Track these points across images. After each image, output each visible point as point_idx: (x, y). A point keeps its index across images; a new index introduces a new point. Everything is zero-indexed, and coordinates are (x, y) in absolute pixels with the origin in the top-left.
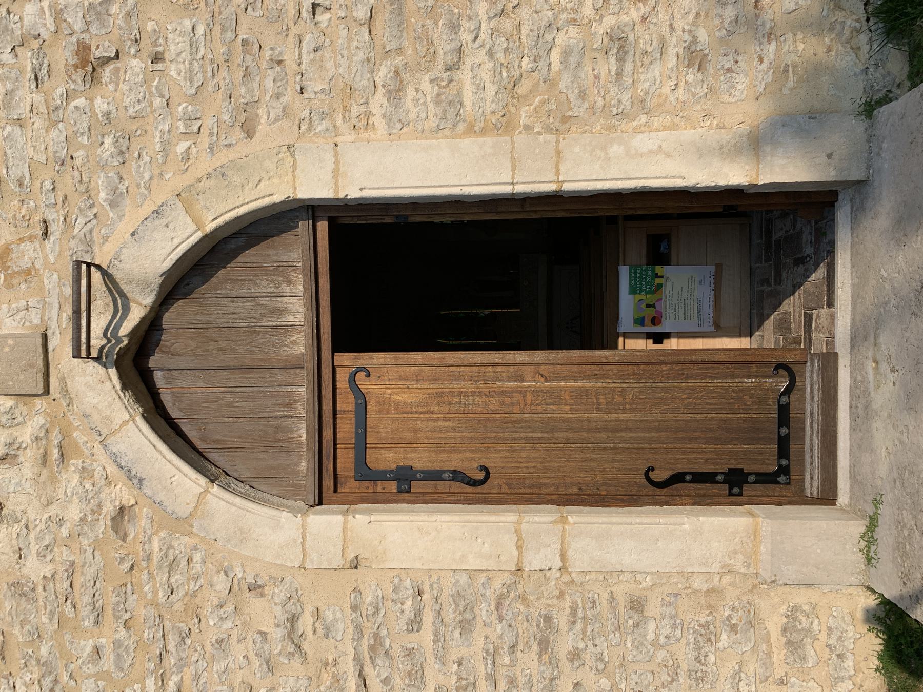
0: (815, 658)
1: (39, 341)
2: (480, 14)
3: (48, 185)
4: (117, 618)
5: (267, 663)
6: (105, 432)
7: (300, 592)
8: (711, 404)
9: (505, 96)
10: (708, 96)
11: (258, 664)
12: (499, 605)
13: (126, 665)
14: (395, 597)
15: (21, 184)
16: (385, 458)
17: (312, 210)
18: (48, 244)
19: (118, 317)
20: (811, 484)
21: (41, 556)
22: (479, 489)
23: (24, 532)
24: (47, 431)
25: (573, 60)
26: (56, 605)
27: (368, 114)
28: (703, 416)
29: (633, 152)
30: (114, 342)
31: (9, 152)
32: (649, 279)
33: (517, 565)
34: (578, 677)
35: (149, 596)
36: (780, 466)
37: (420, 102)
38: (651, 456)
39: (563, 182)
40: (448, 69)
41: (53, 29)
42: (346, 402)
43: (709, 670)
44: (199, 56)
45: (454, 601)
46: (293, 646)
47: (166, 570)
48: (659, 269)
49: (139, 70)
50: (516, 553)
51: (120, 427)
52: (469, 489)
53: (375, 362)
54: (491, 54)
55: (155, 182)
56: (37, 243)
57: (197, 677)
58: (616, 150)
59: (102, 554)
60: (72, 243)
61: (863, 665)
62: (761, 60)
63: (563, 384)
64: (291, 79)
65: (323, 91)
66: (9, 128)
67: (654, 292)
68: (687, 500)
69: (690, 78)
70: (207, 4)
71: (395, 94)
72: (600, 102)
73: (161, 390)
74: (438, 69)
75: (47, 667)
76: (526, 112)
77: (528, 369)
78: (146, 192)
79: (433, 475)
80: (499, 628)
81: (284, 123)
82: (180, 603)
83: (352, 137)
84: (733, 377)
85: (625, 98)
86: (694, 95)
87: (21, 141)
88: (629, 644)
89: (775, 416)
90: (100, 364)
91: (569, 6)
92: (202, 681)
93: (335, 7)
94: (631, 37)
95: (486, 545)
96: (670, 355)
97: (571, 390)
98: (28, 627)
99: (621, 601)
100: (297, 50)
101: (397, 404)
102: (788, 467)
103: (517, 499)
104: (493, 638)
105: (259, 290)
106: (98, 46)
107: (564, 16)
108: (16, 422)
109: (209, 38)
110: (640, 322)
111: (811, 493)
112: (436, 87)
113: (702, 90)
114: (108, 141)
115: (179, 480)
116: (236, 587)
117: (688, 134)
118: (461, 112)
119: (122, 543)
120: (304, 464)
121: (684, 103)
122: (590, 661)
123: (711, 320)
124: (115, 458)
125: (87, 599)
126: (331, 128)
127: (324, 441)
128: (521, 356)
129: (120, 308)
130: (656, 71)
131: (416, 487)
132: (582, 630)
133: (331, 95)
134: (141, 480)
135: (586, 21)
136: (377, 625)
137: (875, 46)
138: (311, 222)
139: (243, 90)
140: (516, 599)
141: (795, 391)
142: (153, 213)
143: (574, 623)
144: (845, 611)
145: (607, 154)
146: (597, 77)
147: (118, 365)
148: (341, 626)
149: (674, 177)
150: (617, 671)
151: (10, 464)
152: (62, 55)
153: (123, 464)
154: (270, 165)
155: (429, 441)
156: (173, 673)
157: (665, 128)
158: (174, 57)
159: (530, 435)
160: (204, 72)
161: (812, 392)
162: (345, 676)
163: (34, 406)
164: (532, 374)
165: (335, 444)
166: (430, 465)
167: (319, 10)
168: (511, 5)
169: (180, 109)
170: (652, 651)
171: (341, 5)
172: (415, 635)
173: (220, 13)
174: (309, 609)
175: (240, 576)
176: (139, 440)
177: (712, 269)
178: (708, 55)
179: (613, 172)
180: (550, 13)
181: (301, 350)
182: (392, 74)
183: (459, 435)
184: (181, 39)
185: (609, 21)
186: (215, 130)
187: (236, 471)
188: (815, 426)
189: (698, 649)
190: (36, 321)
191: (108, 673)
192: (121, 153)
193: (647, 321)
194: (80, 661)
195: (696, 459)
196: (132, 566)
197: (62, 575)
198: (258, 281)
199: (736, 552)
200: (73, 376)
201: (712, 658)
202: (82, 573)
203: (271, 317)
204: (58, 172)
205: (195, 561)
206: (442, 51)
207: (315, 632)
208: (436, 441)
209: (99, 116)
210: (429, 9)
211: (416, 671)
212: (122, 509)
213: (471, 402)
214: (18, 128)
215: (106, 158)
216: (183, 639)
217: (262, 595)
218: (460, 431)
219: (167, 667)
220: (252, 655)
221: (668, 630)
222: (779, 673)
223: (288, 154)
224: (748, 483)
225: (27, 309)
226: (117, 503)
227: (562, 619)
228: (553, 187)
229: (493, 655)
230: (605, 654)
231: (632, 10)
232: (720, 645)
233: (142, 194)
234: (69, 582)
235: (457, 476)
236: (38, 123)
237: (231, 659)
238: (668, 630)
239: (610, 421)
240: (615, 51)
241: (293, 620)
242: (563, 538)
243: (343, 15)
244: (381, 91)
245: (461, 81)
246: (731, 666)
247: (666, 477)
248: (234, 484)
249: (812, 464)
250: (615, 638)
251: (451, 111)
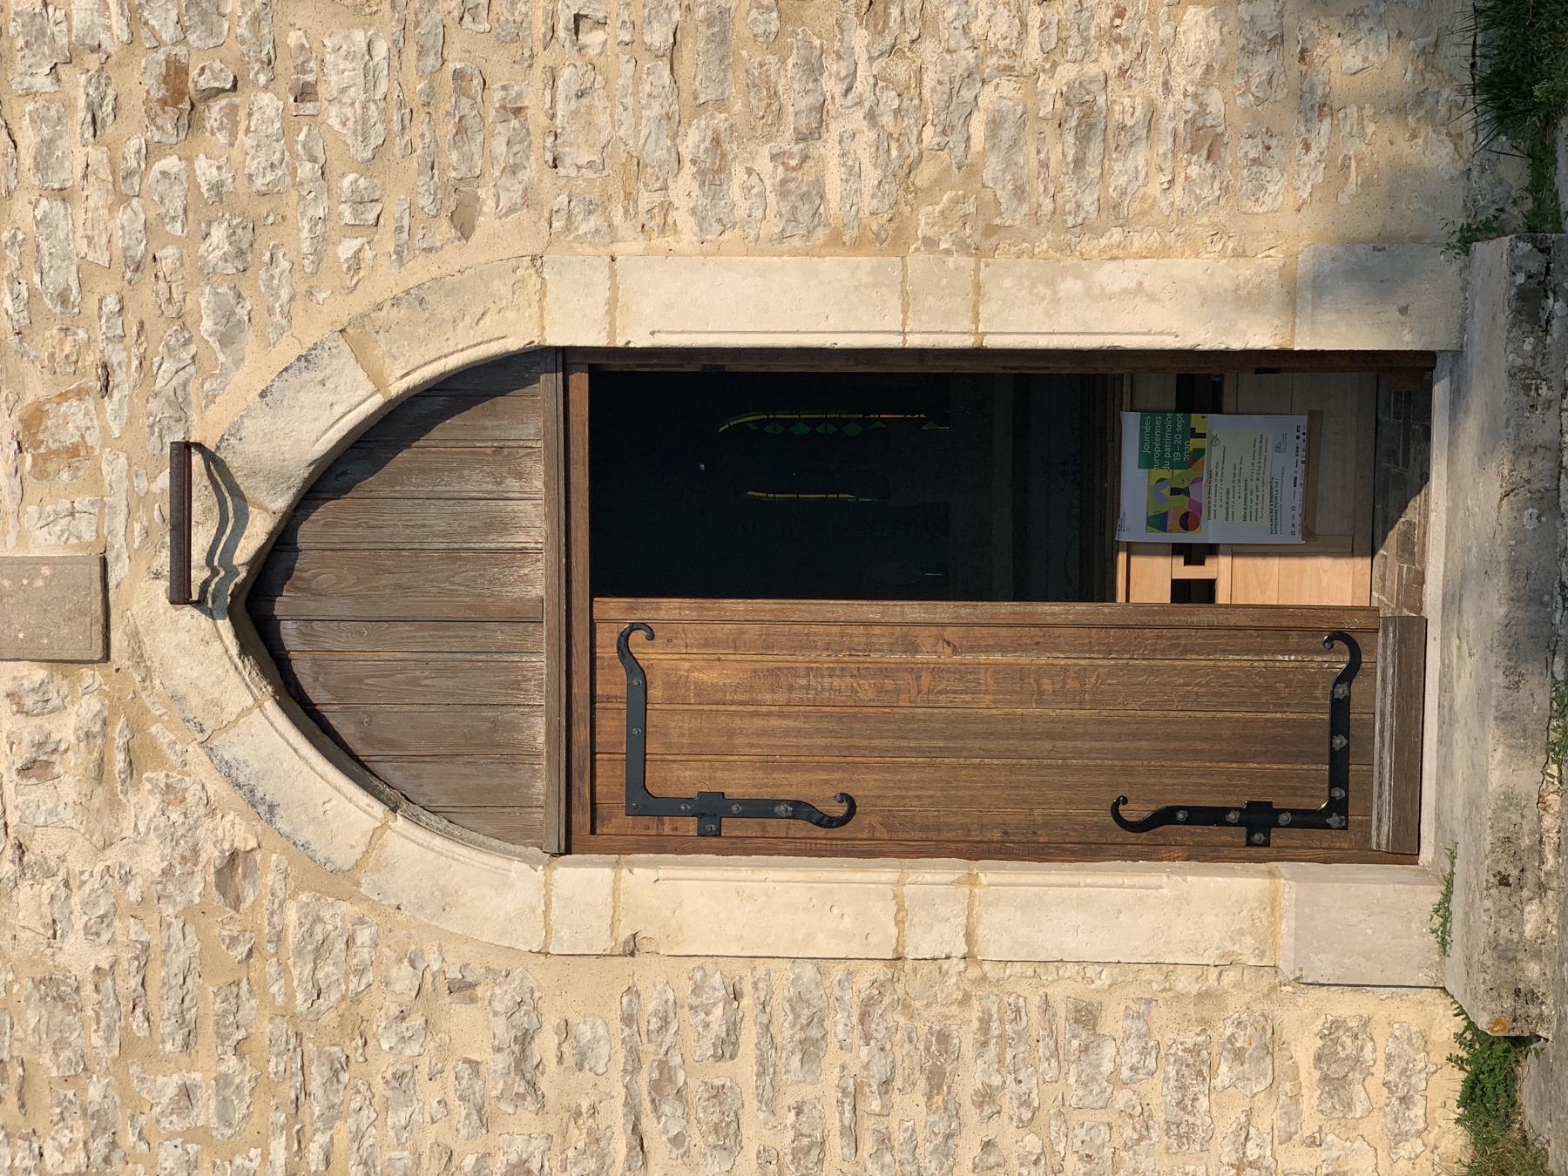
0: (1367, 1104)
1: (97, 570)
2: (857, 50)
3: (111, 304)
4: (223, 1038)
5: (479, 1111)
6: (209, 725)
7: (537, 995)
8: (1223, 695)
9: (894, 188)
10: (1222, 202)
11: (464, 1113)
12: (864, 1016)
13: (238, 1116)
14: (695, 1001)
15: (63, 298)
16: (678, 777)
17: (564, 358)
18: (109, 405)
19: (228, 531)
20: (1379, 828)
21: (91, 933)
22: (837, 832)
23: (63, 892)
24: (104, 723)
25: (1006, 135)
26: (116, 1016)
27: (667, 207)
28: (1210, 714)
29: (1097, 290)
30: (222, 573)
31: (44, 245)
32: (1178, 440)
33: (896, 950)
34: (990, 1131)
35: (280, 1000)
36: (1332, 800)
37: (754, 191)
38: (1123, 779)
39: (986, 333)
40: (801, 138)
41: (125, 37)
42: (612, 682)
43: (1199, 1122)
44: (379, 95)
45: (793, 1009)
46: (523, 1083)
47: (310, 957)
48: (1197, 420)
49: (273, 113)
50: (895, 931)
51: (238, 718)
52: (821, 832)
53: (663, 615)
54: (872, 117)
55: (298, 305)
56: (90, 403)
57: (358, 1136)
58: (1070, 286)
59: (197, 932)
60: (154, 405)
63: (983, 658)
64: (537, 142)
65: (591, 164)
66: (44, 203)
68: (1179, 851)
69: (1194, 171)
70: (393, 7)
71: (713, 175)
72: (1048, 205)
73: (292, 655)
74: (785, 140)
75: (99, 1121)
76: (928, 215)
77: (926, 632)
78: (284, 322)
79: (760, 809)
81: (523, 215)
82: (332, 1014)
83: (637, 246)
84: (1259, 652)
85: (1089, 200)
86: (1198, 199)
87: (64, 227)
88: (1072, 1080)
89: (1327, 717)
90: (202, 611)
91: (1002, 45)
92: (367, 1142)
93: (614, 23)
94: (1101, 100)
95: (846, 918)
96: (1156, 613)
97: (996, 669)
98: (66, 1054)
99: (1062, 1010)
100: (548, 92)
101: (700, 689)
103: (902, 848)
104: (854, 1068)
106: (203, 69)
107: (993, 61)
108: (50, 706)
109: (395, 63)
111: (1378, 845)
112: (781, 169)
114: (218, 233)
115: (337, 808)
116: (428, 987)
117: (1187, 267)
118: (822, 210)
119: (232, 913)
121: (1182, 211)
123: (1298, 521)
124: (227, 770)
125: (170, 1006)
126: (604, 228)
127: (575, 748)
129: (231, 515)
130: (1139, 157)
131: (731, 827)
132: (998, 1056)
133: (605, 173)
134: (272, 808)
135: (1028, 70)
136: (664, 1048)
137: (1481, 138)
138: (560, 375)
140: (892, 1006)
141: (1359, 676)
142: (299, 359)
143: (985, 1044)
144: (1414, 1029)
145: (1056, 293)
146: (1044, 165)
149: (1161, 333)
150: (1053, 1122)
151: (38, 777)
152: (140, 82)
153: (242, 779)
154: (501, 288)
155: (754, 751)
156: (317, 1130)
158: (335, 94)
159: (925, 744)
160: (388, 122)
161: (1384, 680)
162: (608, 1134)
163: (80, 680)
164: (932, 640)
165: (593, 754)
166: (755, 790)
167: (584, 25)
168: (908, 38)
170: (1109, 1090)
171: (624, 22)
172: (726, 1065)
173: (417, 24)
174: (551, 1021)
175: (435, 968)
176: (269, 739)
177: (1303, 420)
178: (1222, 134)
179: (1065, 322)
180: (970, 55)
181: (538, 590)
182: (707, 144)
183: (805, 742)
184: (349, 66)
185: (1067, 72)
186: (406, 222)
187: (424, 794)
188: (1387, 735)
189: (1182, 1088)
190: (88, 536)
191: (205, 1128)
192: (241, 253)
193: (1173, 521)
194: (158, 1109)
195: (1195, 784)
196: (251, 951)
197: (127, 964)
198: (466, 472)
199: (1241, 933)
200: (155, 631)
201: (1203, 1103)
202: (164, 963)
203: (488, 534)
204: (130, 282)
205: (359, 942)
206: (791, 109)
207: (560, 1060)
208: (766, 751)
209: (204, 189)
210: (772, 37)
211: (728, 1124)
212: (234, 855)
213: (827, 685)
214: (60, 204)
215: (214, 261)
216: (336, 1073)
217: (473, 1000)
218: (808, 735)
219: (308, 1120)
220: (452, 1099)
221: (1135, 1058)
222: (1309, 1127)
223: (532, 271)
224: (1279, 826)
225: (72, 514)
226: (227, 846)
227: (965, 1039)
228: (967, 342)
229: (854, 1095)
230: (1034, 1095)
231: (1104, 55)
232: (1217, 1082)
233: (277, 326)
234: (139, 978)
235: (800, 809)
236: (96, 196)
237: (416, 1106)
238: (1135, 1058)
240: (1074, 123)
241: (525, 1039)
242: (970, 906)
243: (627, 39)
244: (689, 169)
246: (1236, 1115)
247: (1147, 814)
248: (425, 817)
249: (1380, 796)
250: (1049, 1069)
251: (805, 210)
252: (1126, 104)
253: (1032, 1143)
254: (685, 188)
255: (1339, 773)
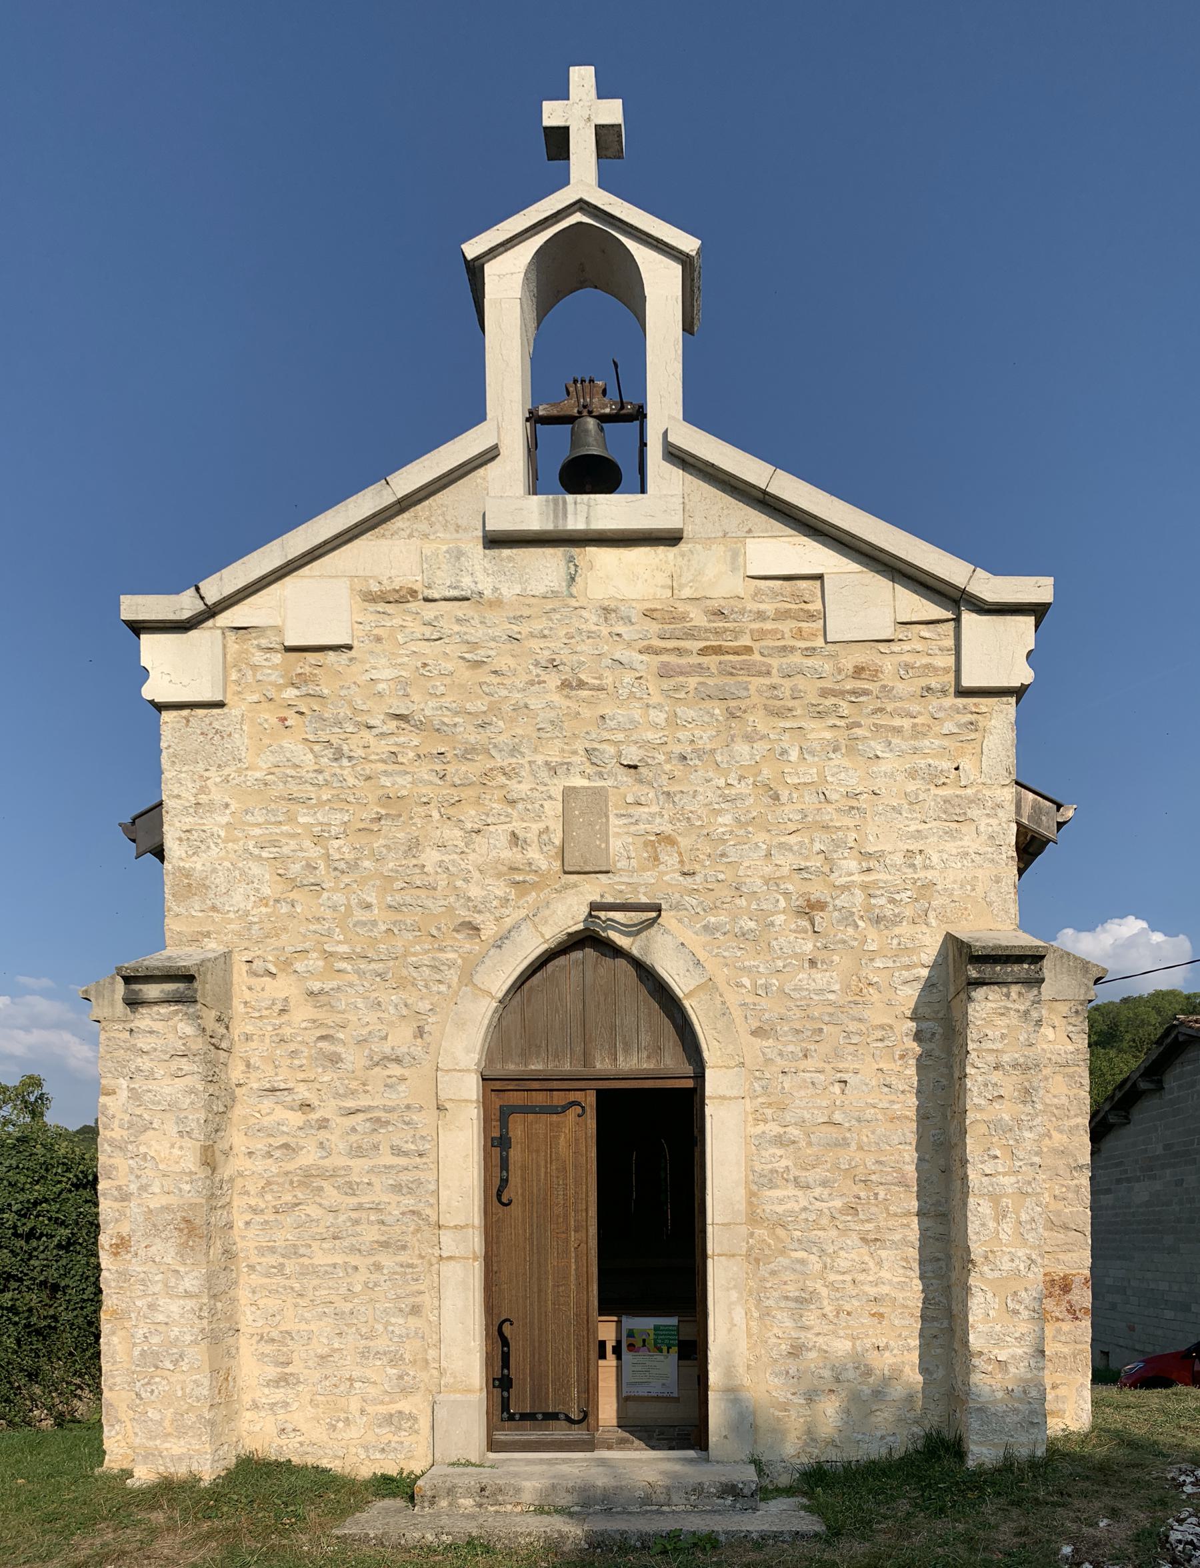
1: (604, 869)
3: (721, 877)
4: (394, 923)
6: (536, 919)
12: (413, 1212)
15: (723, 855)
16: (518, 1128)
17: (700, 1077)
18: (677, 875)
22: (495, 1198)
23: (459, 851)
25: (798, 1266)
27: (765, 1121)
34: (362, 1269)
36: (514, 1414)
44: (812, 996)
48: (675, 1349)
52: (495, 1191)
54: (805, 1209)
55: (722, 960)
56: (678, 866)
57: (351, 985)
58: (734, 1295)
60: (677, 895)
61: (377, 1465)
62: (794, 1394)
67: (655, 1346)
69: (783, 1347)
71: (779, 1141)
72: (769, 1285)
74: (795, 1172)
75: (354, 866)
77: (584, 1235)
79: (504, 1164)
80: (396, 1212)
81: (761, 1059)
83: (749, 1109)
85: (771, 1303)
92: (348, 989)
94: (812, 1307)
98: (384, 851)
99: (418, 1299)
101: (558, 1137)
102: (514, 1420)
104: (389, 1208)
105: (643, 1036)
107: (829, 1261)
110: (631, 1334)
113: (774, 1354)
114: (752, 925)
115: (501, 976)
116: (420, 1017)
117: (743, 1345)
120: (512, 1067)
122: (374, 1277)
124: (516, 927)
125: (408, 899)
128: (593, 1230)
130: (789, 1323)
139: (786, 1029)
143: (402, 1266)
147: (586, 929)
148: (394, 1096)
152: (818, 891)
157: (748, 1329)
169: (774, 981)
172: (389, 1151)
176: (530, 947)
179: (719, 1294)
181: (598, 1066)
185: (824, 1292)
189: (385, 1354)
190: (619, 865)
193: (631, 1340)
197: (427, 880)
199: (455, 1377)
201: (378, 1363)
207: (389, 1077)
216: (380, 975)
220: (370, 1028)
222: (369, 1409)
227: (403, 1257)
228: (709, 1252)
232: (388, 1369)
235: (504, 1182)
236: (768, 870)
237: (366, 1012)
239: (546, 1294)
241: (398, 1060)
244: (781, 1130)
245: (787, 1188)
250: (391, 1295)
252: (811, 1318)
253: (358, 1288)
254: (773, 1129)
255: (524, 1417)
